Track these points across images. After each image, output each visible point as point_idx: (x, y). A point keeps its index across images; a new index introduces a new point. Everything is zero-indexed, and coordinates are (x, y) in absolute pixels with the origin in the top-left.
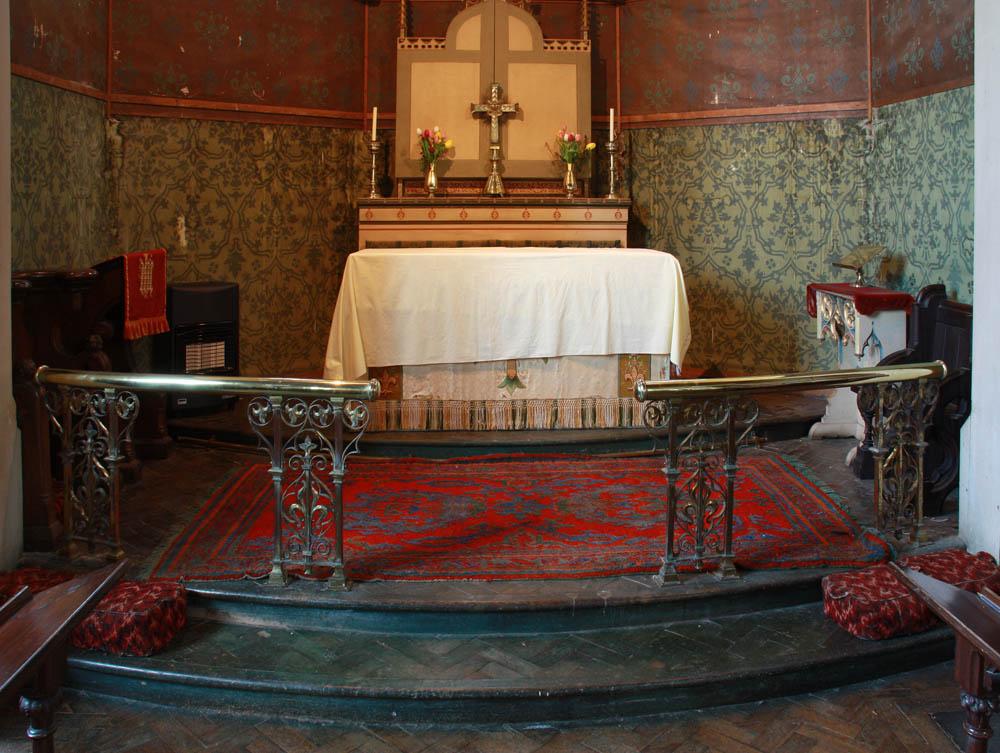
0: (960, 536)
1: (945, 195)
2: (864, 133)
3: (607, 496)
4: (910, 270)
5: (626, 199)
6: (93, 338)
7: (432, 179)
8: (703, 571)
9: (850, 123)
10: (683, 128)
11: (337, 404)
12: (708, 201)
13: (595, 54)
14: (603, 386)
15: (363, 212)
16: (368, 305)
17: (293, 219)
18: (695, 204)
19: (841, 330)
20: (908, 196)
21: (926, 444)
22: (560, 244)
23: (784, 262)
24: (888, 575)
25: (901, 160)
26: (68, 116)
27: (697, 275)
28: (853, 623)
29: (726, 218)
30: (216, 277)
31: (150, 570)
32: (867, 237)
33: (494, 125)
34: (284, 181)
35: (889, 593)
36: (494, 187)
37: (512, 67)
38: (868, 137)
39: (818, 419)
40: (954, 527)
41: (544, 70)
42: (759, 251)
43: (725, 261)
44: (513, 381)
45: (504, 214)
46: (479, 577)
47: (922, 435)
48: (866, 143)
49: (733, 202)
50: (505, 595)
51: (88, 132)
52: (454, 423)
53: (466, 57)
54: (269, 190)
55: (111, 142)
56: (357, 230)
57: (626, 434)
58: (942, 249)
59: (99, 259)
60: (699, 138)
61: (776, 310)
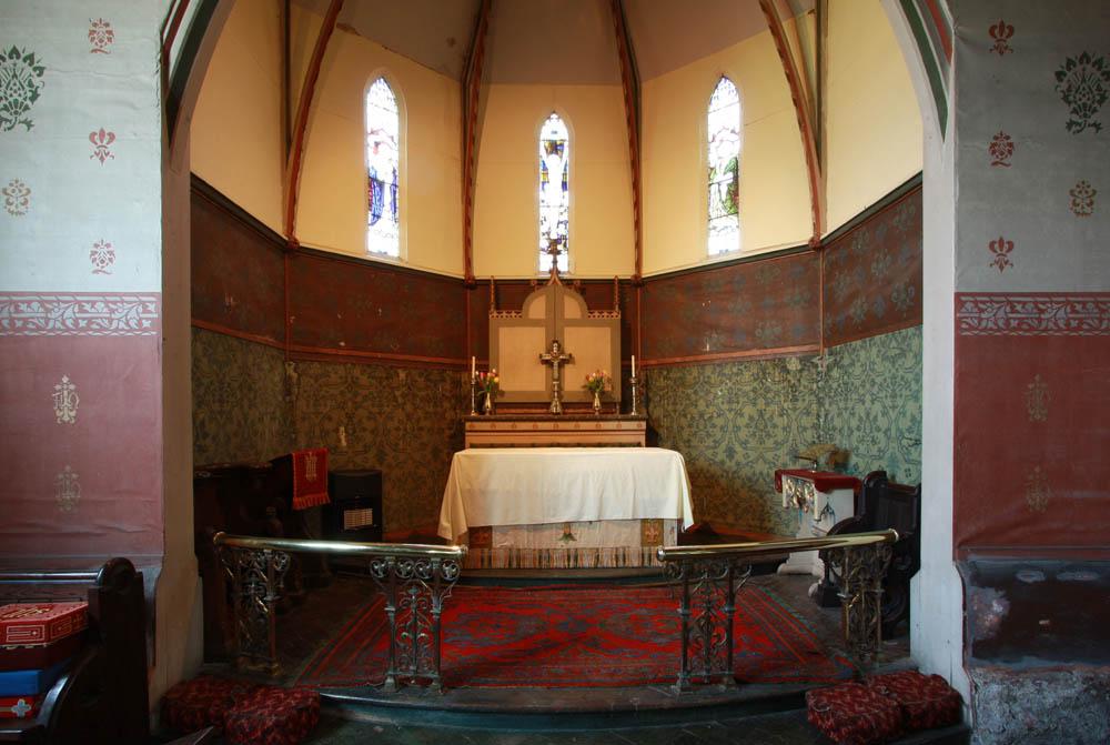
0: (911, 658)
1: (884, 407)
2: (817, 366)
3: (634, 618)
4: (854, 460)
5: (645, 415)
6: (268, 509)
7: (597, 403)
8: (711, 683)
9: (806, 360)
10: (684, 368)
11: (436, 562)
12: (702, 415)
13: (623, 321)
14: (631, 540)
15: (468, 424)
16: (468, 487)
17: (421, 429)
18: (692, 418)
19: (801, 501)
20: (903, 406)
21: (883, 591)
22: (600, 445)
23: (756, 455)
24: (860, 692)
25: (847, 384)
26: (255, 359)
27: (694, 464)
28: (834, 731)
29: (714, 426)
30: (368, 466)
31: (296, 679)
32: (819, 437)
33: (556, 368)
34: (414, 404)
35: (862, 709)
36: (555, 408)
37: (567, 329)
38: (820, 369)
39: (784, 561)
40: (906, 650)
41: (588, 332)
42: (738, 448)
43: (714, 454)
44: (568, 536)
45: (562, 425)
46: (542, 684)
47: (879, 583)
48: (818, 373)
49: (719, 416)
50: (560, 700)
51: (272, 369)
52: (527, 564)
53: (536, 323)
54: (403, 409)
55: (290, 377)
56: (464, 435)
57: (646, 572)
58: (882, 445)
59: (272, 457)
60: (695, 373)
61: (750, 487)
